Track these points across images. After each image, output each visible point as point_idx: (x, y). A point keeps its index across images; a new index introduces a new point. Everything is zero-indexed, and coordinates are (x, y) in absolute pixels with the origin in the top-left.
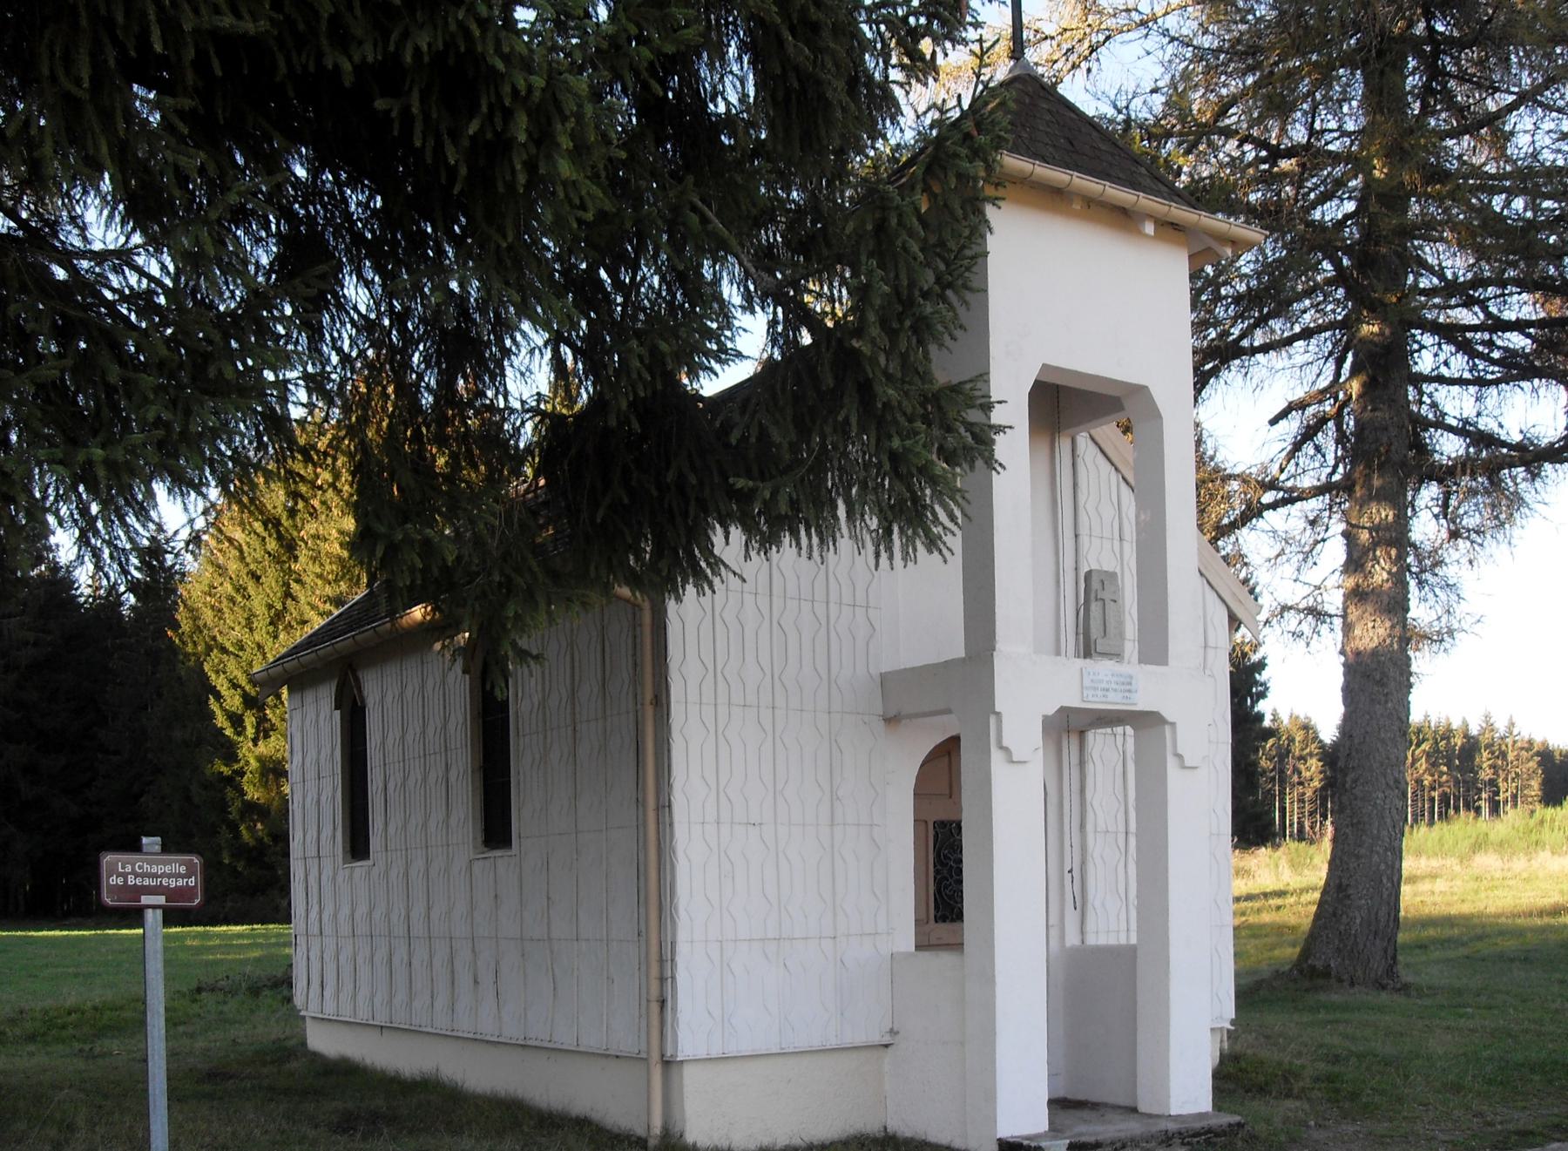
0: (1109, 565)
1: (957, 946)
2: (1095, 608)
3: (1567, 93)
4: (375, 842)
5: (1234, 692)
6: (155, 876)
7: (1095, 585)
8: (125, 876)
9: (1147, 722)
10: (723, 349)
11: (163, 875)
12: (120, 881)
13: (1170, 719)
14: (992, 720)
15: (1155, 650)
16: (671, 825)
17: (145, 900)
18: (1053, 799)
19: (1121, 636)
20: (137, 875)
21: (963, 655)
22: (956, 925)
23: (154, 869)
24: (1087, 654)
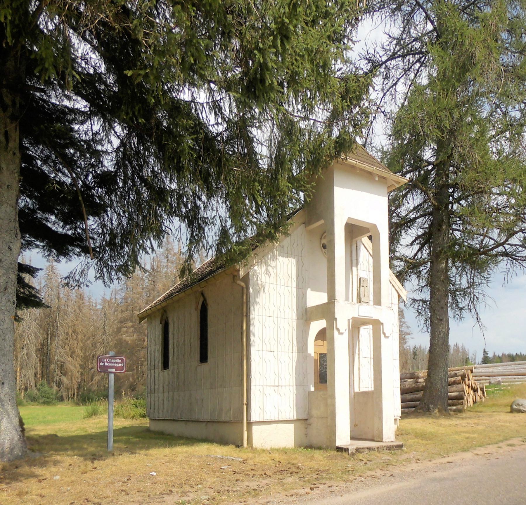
0: (366, 277)
1: (326, 389)
2: (362, 288)
3: (443, 504)
4: (170, 363)
5: (400, 343)
6: (113, 363)
7: (362, 282)
8: (104, 362)
9: (377, 324)
10: (260, 126)
11: (115, 363)
12: (103, 364)
13: (382, 322)
14: (335, 322)
15: (378, 302)
16: (248, 345)
17: (110, 370)
18: (351, 346)
19: (369, 297)
20: (107, 363)
21: (326, 301)
22: (325, 384)
23: (112, 361)
24: (360, 302)
